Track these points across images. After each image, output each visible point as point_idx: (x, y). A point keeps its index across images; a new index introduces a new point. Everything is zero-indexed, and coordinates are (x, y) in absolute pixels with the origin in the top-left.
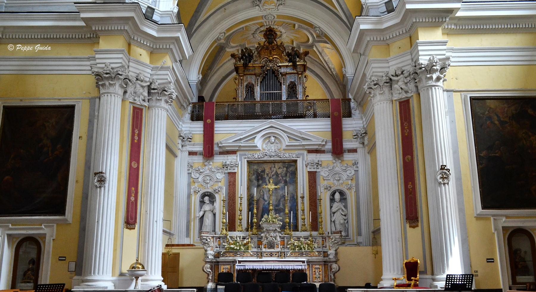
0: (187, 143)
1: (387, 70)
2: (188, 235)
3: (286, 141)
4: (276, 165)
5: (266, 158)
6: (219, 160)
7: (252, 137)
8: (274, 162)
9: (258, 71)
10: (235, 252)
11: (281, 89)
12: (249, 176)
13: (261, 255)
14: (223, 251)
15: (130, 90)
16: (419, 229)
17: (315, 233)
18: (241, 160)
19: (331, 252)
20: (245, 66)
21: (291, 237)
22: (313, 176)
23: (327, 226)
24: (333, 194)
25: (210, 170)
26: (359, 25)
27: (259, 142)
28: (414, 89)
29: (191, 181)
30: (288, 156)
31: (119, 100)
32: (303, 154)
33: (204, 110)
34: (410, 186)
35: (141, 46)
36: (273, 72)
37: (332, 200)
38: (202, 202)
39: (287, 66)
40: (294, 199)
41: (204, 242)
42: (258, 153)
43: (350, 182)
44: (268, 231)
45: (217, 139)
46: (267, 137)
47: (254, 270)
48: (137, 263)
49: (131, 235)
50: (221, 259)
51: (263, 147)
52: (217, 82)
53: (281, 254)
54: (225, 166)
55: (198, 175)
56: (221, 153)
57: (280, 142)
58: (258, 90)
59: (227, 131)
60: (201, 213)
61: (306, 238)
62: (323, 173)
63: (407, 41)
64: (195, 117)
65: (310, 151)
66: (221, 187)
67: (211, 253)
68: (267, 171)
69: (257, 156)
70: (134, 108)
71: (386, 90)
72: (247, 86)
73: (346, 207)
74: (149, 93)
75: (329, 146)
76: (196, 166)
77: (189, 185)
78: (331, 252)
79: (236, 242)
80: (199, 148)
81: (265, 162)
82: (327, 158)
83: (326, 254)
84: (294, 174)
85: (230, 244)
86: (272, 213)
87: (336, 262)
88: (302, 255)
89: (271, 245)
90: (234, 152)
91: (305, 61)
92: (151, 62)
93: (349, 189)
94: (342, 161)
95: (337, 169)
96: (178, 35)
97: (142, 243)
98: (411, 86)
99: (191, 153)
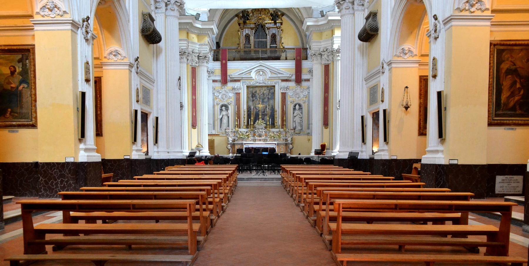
0: (212, 75)
1: (320, 47)
2: (214, 129)
3: (269, 75)
4: (264, 88)
5: (257, 85)
6: (230, 85)
7: (250, 72)
8: (262, 87)
9: (253, 26)
10: (243, 139)
11: (266, 38)
12: (247, 95)
13: (255, 140)
14: (237, 138)
15: (190, 58)
16: (328, 129)
17: (282, 130)
18: (243, 85)
19: (289, 139)
20: (245, 23)
21: (270, 131)
22: (284, 95)
23: (290, 124)
24: (295, 106)
25: (225, 91)
26: (306, 23)
27: (253, 75)
28: (332, 60)
29: (215, 98)
30: (269, 83)
31: (185, 65)
32: (278, 82)
33: (220, 54)
34: (326, 109)
35: (193, 33)
36: (262, 27)
37: (294, 109)
38: (221, 110)
39: (270, 23)
40: (273, 110)
41: (227, 134)
42: (253, 81)
43: (305, 99)
44: (259, 129)
45: (229, 73)
46: (258, 72)
47: (252, 148)
48: (199, 144)
49: (195, 131)
50: (236, 142)
51: (256, 78)
52: (224, 24)
53: (265, 140)
54: (234, 89)
55: (218, 94)
56: (231, 81)
57: (266, 75)
58: (252, 38)
59: (236, 68)
60: (221, 116)
61: (277, 132)
62: (290, 93)
63: (330, 32)
64: (216, 59)
65: (283, 80)
66: (232, 101)
67: (231, 139)
68: (258, 92)
69: (252, 83)
70: (192, 68)
71: (319, 58)
72: (245, 36)
73: (302, 113)
74: (198, 59)
75: (294, 77)
76: (217, 89)
77: (214, 100)
78: (289, 139)
79: (243, 134)
80: (219, 78)
81: (257, 87)
82: (292, 84)
83: (286, 140)
84: (274, 94)
85: (240, 135)
86: (260, 120)
87: (291, 144)
88: (275, 140)
89: (260, 136)
90: (239, 81)
91: (281, 20)
92: (198, 41)
93: (304, 103)
94: (301, 86)
95: (298, 91)
96: (212, 27)
97: (199, 135)
98: (330, 57)
99: (214, 81)
